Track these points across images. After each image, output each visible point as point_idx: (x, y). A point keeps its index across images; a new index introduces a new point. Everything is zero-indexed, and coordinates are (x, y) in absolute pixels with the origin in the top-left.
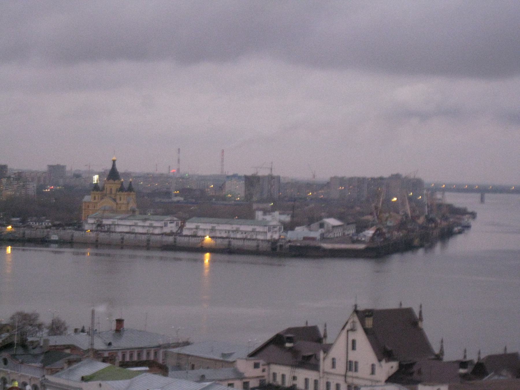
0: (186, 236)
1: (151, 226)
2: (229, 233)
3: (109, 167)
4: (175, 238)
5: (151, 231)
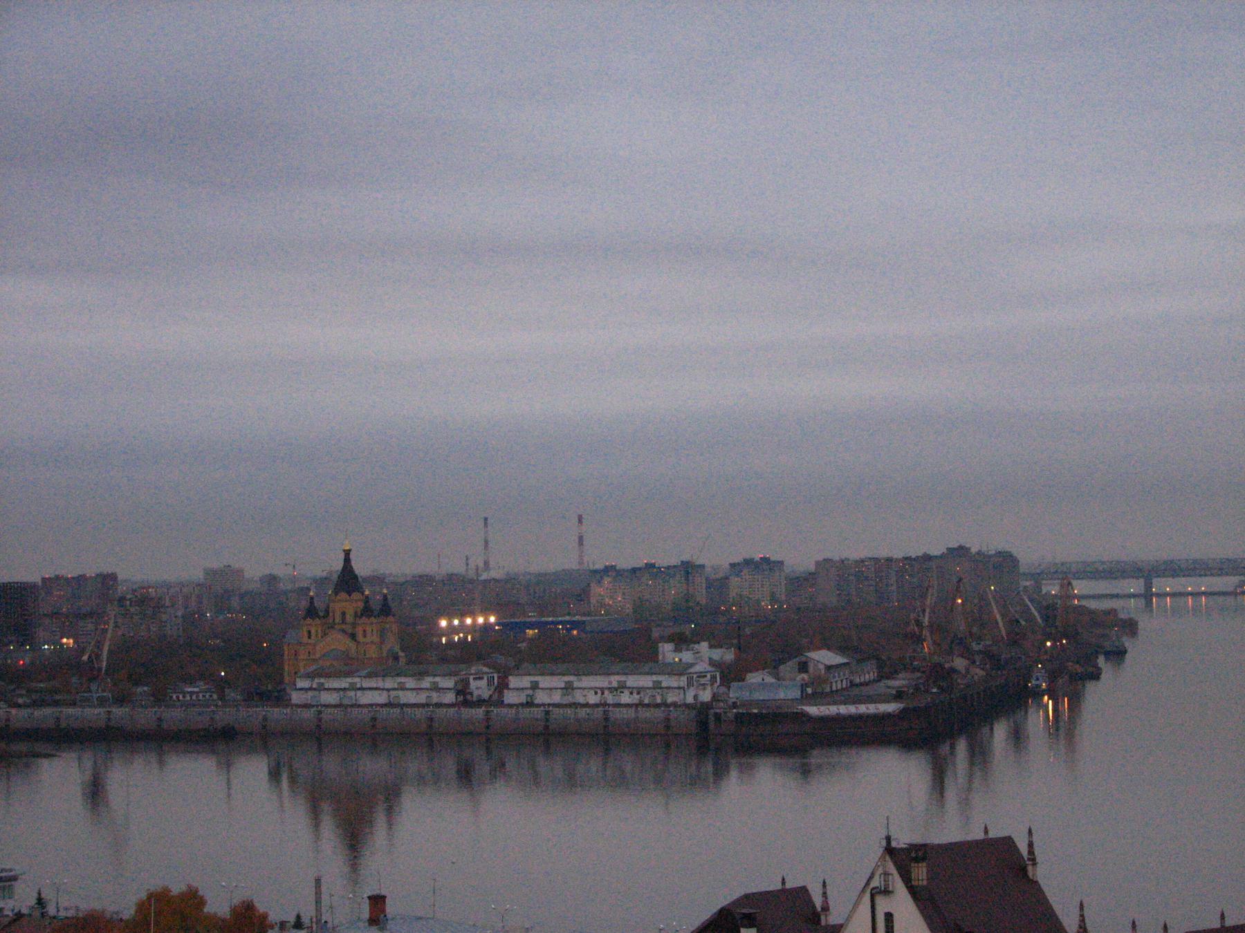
1: (436, 688)
3: (339, 565)
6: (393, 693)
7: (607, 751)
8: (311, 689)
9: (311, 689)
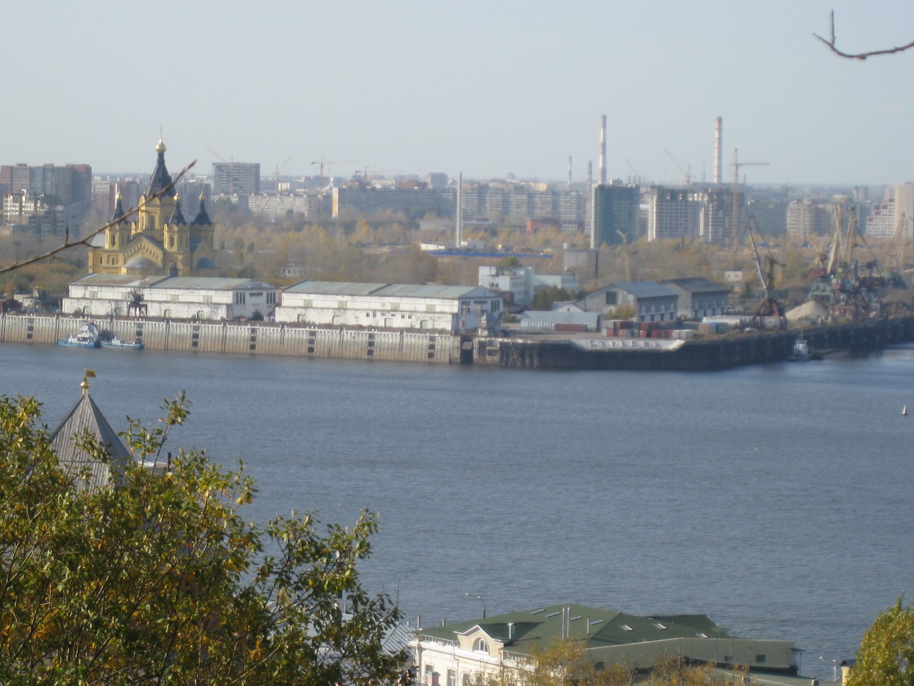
0: (283, 324)
1: (430, 311)
2: (374, 315)
3: (150, 168)
4: (253, 331)
5: (206, 312)
6: (164, 307)
7: (166, 344)
8: (84, 298)
9: (84, 298)
